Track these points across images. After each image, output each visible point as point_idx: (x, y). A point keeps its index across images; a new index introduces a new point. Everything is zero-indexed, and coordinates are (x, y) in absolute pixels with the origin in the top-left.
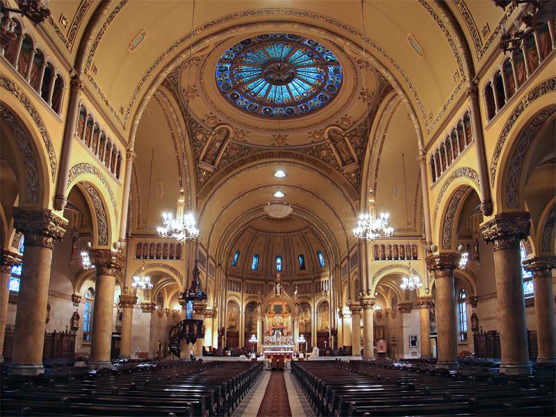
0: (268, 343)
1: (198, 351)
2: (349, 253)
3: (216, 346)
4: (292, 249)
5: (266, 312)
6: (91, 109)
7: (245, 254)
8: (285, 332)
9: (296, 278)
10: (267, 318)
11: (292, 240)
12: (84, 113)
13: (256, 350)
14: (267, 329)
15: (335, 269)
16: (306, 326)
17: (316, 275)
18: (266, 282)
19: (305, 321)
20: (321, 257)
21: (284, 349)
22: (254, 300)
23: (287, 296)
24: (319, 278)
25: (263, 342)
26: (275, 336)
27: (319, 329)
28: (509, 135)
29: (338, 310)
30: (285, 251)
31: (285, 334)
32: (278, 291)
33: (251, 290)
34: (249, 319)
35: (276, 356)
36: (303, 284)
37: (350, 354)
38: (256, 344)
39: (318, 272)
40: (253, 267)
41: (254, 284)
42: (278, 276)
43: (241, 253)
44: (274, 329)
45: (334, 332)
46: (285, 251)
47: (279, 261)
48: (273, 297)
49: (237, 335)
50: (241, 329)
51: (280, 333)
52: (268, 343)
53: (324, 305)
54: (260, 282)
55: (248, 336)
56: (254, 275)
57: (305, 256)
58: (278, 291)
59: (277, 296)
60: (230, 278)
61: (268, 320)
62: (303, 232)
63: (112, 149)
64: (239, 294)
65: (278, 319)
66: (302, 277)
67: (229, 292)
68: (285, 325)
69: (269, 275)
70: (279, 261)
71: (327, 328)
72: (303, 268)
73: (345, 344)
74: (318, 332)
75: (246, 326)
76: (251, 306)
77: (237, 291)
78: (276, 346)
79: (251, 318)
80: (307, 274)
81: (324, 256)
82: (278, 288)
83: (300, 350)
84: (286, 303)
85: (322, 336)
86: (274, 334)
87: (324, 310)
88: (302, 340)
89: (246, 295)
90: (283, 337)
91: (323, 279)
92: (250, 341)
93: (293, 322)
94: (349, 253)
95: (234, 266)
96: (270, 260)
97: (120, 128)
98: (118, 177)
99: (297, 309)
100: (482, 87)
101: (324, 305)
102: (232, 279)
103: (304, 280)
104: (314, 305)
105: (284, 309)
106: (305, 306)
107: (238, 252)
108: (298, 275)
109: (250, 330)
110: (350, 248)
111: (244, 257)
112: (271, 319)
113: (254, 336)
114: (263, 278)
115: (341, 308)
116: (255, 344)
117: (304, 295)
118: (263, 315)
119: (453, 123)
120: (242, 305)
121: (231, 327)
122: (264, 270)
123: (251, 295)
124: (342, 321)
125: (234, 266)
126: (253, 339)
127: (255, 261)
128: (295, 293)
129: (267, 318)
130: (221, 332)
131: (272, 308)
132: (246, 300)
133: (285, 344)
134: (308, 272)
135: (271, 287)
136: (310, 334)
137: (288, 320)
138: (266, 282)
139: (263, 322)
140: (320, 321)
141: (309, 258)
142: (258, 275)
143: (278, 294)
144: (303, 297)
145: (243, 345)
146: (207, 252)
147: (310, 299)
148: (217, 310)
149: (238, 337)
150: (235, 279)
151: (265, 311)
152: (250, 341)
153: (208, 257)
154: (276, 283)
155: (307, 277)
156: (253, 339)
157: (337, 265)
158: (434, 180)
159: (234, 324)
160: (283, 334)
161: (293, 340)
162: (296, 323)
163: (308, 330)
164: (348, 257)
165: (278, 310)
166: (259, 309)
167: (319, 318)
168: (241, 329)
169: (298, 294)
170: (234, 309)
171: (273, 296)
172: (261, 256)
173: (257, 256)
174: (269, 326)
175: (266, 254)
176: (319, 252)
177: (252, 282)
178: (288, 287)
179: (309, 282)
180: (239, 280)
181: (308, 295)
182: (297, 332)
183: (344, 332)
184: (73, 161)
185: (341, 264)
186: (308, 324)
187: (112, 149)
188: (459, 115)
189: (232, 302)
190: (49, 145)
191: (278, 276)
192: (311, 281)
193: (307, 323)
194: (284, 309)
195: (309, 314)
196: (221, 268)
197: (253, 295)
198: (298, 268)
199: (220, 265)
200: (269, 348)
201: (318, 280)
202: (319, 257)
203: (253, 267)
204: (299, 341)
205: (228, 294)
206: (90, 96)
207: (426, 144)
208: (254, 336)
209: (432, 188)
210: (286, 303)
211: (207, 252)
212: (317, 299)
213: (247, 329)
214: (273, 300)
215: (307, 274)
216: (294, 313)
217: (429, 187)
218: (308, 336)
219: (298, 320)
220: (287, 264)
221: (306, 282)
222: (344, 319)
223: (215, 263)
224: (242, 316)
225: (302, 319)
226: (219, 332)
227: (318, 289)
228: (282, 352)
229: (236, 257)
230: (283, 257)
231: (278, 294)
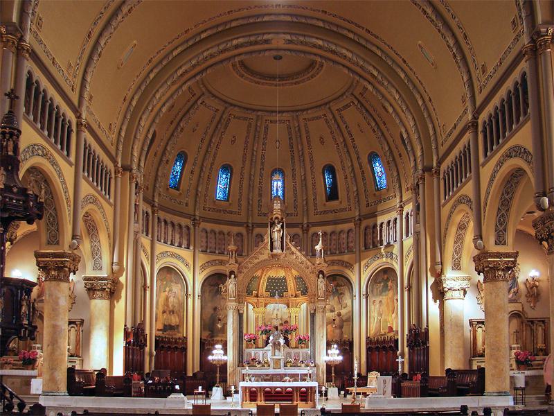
0: (253, 362)
1: (52, 380)
2: (477, 113)
3: (118, 370)
4: (306, 151)
5: (249, 293)
6: (38, 75)
7: (199, 162)
8: (293, 339)
9: (314, 218)
10: (250, 307)
11: (307, 132)
12: (29, 80)
13: (224, 380)
14: (252, 330)
15: (423, 178)
16: (341, 327)
17: (365, 211)
18: (250, 228)
19: (339, 315)
20: (378, 168)
21: (294, 377)
22: (220, 268)
23: (298, 255)
24: (374, 215)
25: (241, 362)
26: (269, 347)
27: (372, 333)
28: (495, 182)
29: (431, 280)
30: (293, 158)
31: (293, 343)
32: (277, 244)
33: (213, 246)
34: (209, 311)
35: (271, 395)
36: (333, 233)
37: (479, 389)
38: (224, 367)
39: (373, 201)
40: (219, 195)
41: (221, 233)
42: (277, 206)
43: (190, 160)
44: (266, 332)
45: (419, 338)
46: (293, 158)
47: (278, 184)
48: (262, 258)
49: (180, 347)
50: (192, 331)
51: (282, 341)
52: (253, 362)
53: (385, 277)
54: (235, 230)
55: (206, 347)
56: (219, 213)
57: (338, 167)
58: (277, 244)
59: (274, 256)
60: (162, 214)
61: (251, 312)
62: (335, 107)
63: (41, 96)
64: (186, 254)
65: (276, 310)
66: (330, 217)
67: (160, 248)
68: (293, 323)
69: (256, 211)
70: (278, 184)
71: (391, 329)
72: (333, 195)
73: (450, 365)
74: (368, 338)
75: (204, 327)
76: (214, 283)
77: (180, 246)
78: (271, 371)
79: (215, 309)
80: (344, 210)
81: (387, 166)
82: (276, 236)
83: (329, 380)
84: (295, 273)
85: (381, 352)
86: (267, 343)
87: (386, 288)
88: (335, 356)
89: (202, 259)
90: (287, 349)
91: (380, 220)
92: (210, 358)
93: (313, 315)
94: (477, 113)
95: (174, 187)
96: (257, 180)
97: (68, 90)
98: (68, 155)
99: (321, 284)
100: (480, 122)
101: (385, 277)
102: (169, 217)
103: (335, 222)
104: (361, 276)
105: (291, 284)
106: (338, 283)
107: (182, 156)
108: (321, 213)
109: (212, 332)
110: (479, 100)
111: (197, 171)
112: (261, 309)
113: (219, 346)
114: (241, 218)
115: (439, 276)
116: (224, 367)
117: (336, 258)
118: (240, 299)
119: (509, 84)
120: (195, 279)
121: (167, 327)
122: (244, 203)
123: (214, 257)
124: (442, 307)
125: (174, 187)
126: (217, 355)
127: (223, 180)
128: (318, 247)
129: (250, 307)
130: (135, 338)
131: (263, 283)
132: (203, 268)
133: (295, 365)
134: (345, 205)
135: (260, 237)
136: (351, 344)
137: (299, 312)
138: (250, 228)
139: (240, 316)
140: (374, 314)
141: (348, 170)
142: (231, 213)
143: (277, 251)
144: (333, 263)
145: (197, 369)
146: (77, 111)
147: (349, 266)
148: (122, 279)
149: (185, 349)
150: (176, 219)
151: (247, 291)
152: (210, 358)
153: (79, 124)
154: (273, 224)
155: (344, 215)
156: (217, 355)
157: (428, 169)
158: (486, 155)
159: (174, 320)
160: (287, 343)
161: (313, 356)
162: (318, 317)
163: (346, 336)
164: (474, 125)
165: (277, 289)
166: (231, 285)
167: (373, 308)
168: (192, 331)
169: (326, 250)
170: (176, 288)
171: (266, 254)
172: (237, 168)
173: (227, 168)
174: (257, 326)
175: (247, 162)
176: (373, 157)
177: (217, 228)
178: (302, 236)
179: (346, 227)
180: (185, 222)
181: (346, 258)
182: (321, 343)
183: (448, 334)
184: (82, 195)
185: (440, 163)
186: (345, 322)
187: (41, 96)
188: (516, 76)
189: (168, 270)
190: (64, 183)
191: (277, 206)
192: (351, 225)
193: (342, 321)
194: (291, 284)
195: (347, 300)
196: (131, 178)
197: (221, 257)
198: (322, 197)
199: (127, 168)
200: (254, 375)
201: (370, 222)
202: (372, 168)
203: (219, 195)
204: (327, 358)
205: (157, 252)
206: (52, 79)
207: (478, 103)
208: (219, 346)
209: (484, 165)
210: (295, 273)
211: (79, 117)
212: (367, 266)
213: (207, 333)
214: (264, 266)
215: (344, 210)
216: (315, 295)
217: (441, 204)
218: (347, 347)
219: (324, 310)
220: (297, 188)
221: (340, 227)
222: (448, 304)
223: (115, 162)
224: (194, 307)
225: (331, 309)
226: (127, 334)
227: (371, 241)
228: (289, 384)
229: (178, 168)
230: (288, 172)
231: (277, 251)
